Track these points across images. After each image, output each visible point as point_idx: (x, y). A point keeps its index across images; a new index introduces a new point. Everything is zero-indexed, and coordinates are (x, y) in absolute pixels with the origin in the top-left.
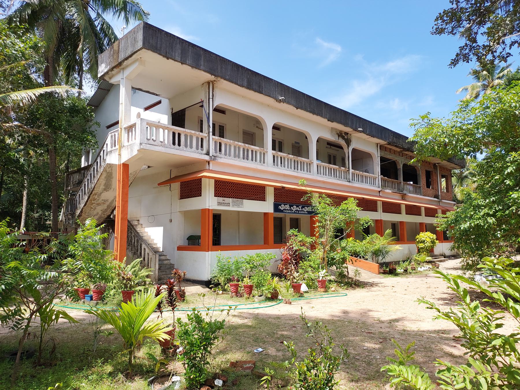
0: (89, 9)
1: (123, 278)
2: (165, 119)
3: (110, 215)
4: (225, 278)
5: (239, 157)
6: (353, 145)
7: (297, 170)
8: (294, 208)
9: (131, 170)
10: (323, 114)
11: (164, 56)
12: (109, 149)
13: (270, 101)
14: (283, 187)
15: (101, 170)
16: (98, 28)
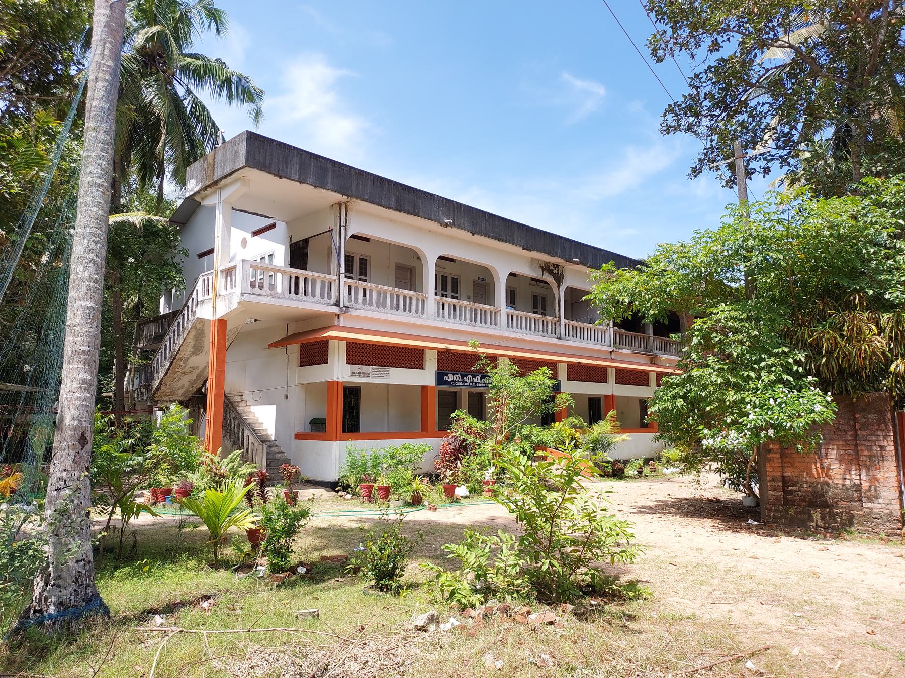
0: (175, 82)
1: (215, 473)
2: (281, 255)
3: (201, 388)
4: (356, 477)
5: (384, 307)
6: (568, 282)
7: (475, 322)
8: (469, 379)
9: (229, 327)
10: (515, 240)
11: (275, 175)
12: (200, 298)
13: (432, 225)
14: (449, 350)
15: (188, 327)
16: (188, 110)
